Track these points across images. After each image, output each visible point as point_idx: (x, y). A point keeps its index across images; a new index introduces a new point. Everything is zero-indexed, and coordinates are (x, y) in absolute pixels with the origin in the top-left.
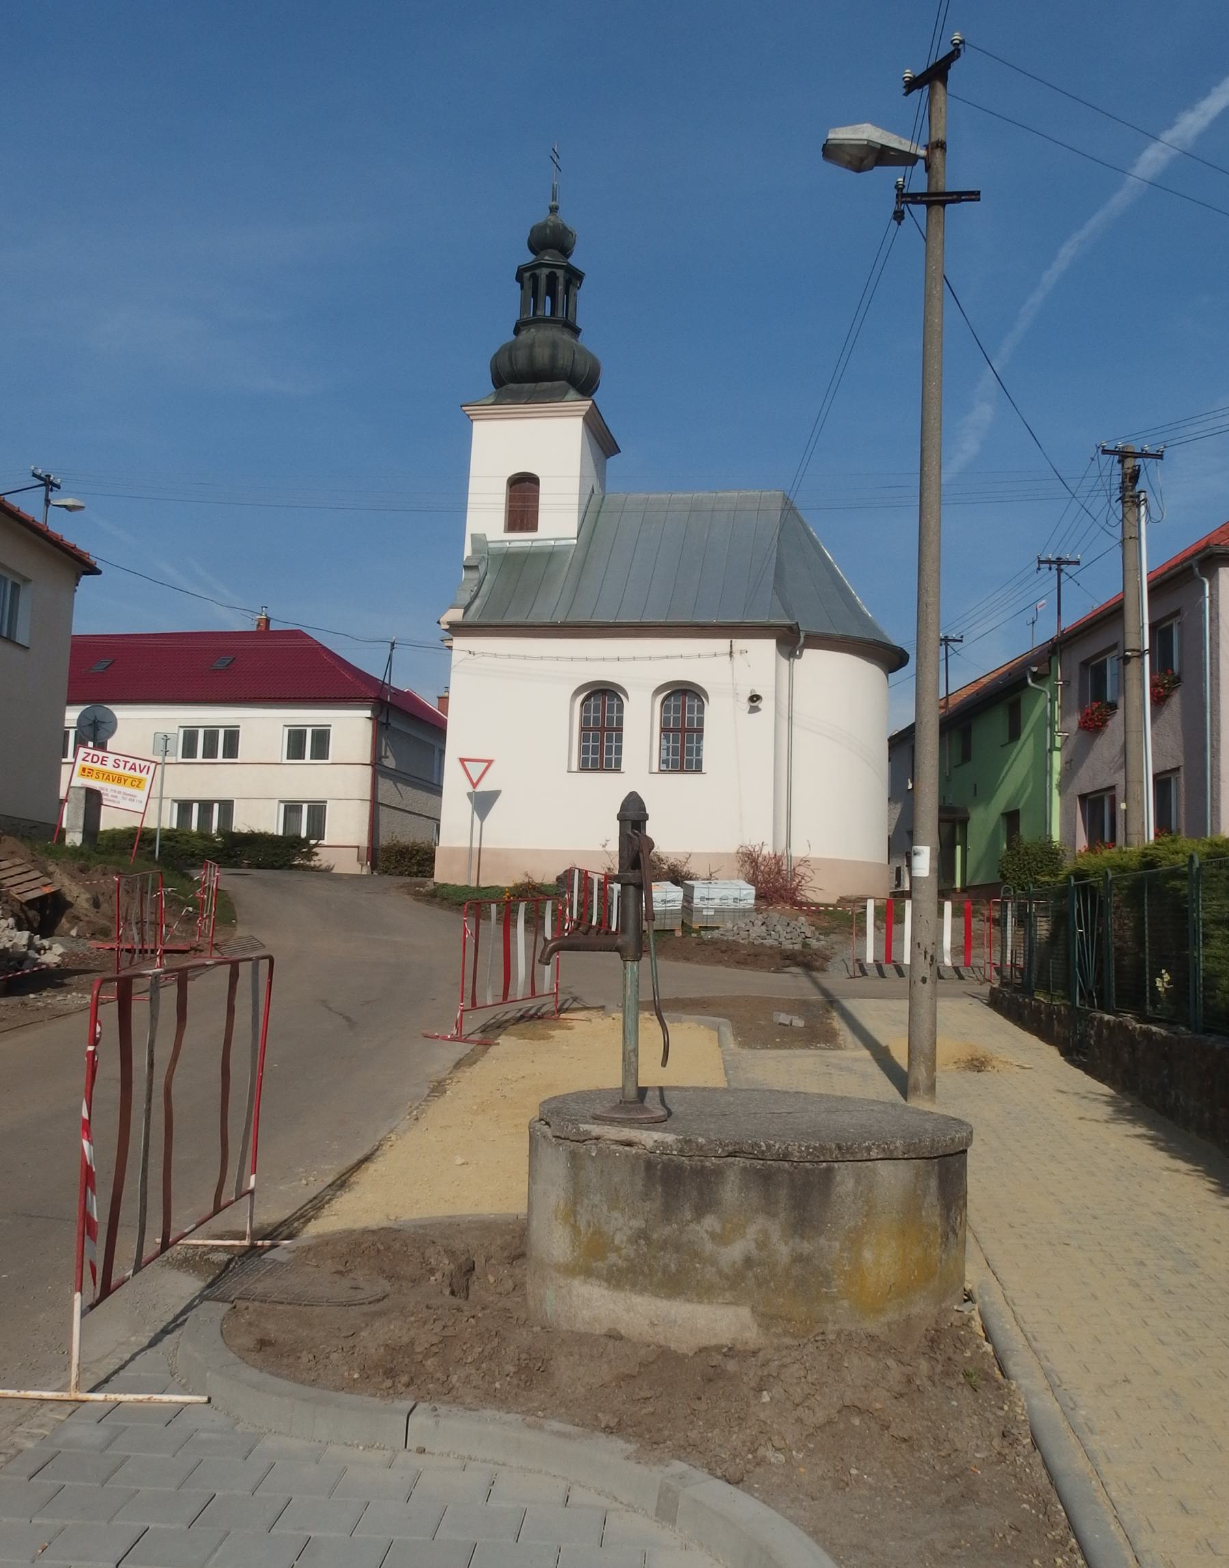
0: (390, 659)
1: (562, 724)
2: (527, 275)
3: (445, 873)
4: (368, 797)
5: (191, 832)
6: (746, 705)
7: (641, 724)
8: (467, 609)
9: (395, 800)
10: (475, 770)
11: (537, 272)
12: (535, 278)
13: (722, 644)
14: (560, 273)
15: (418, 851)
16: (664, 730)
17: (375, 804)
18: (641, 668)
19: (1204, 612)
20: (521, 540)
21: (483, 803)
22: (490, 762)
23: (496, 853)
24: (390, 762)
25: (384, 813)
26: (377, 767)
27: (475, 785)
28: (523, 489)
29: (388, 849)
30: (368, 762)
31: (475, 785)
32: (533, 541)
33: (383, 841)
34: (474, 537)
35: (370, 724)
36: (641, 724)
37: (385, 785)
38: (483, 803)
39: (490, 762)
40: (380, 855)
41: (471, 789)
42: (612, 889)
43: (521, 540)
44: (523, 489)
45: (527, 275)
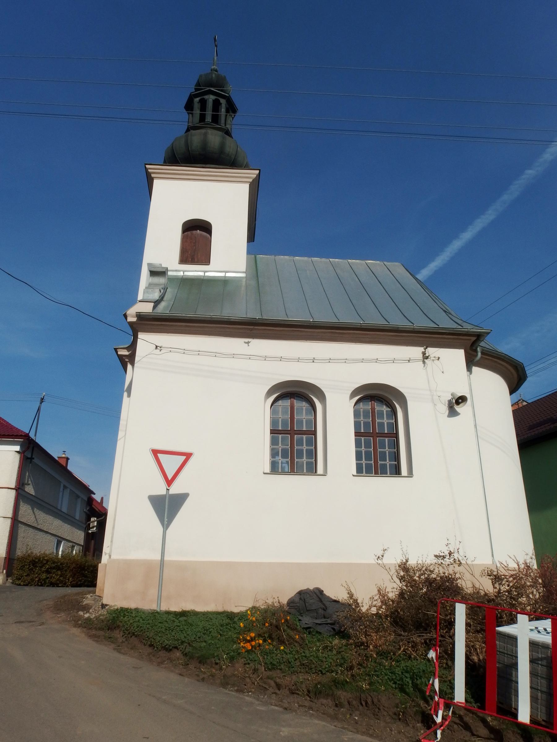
0: (39, 410)
1: (257, 419)
2: (197, 99)
3: (115, 589)
4: (10, 514)
5: (58, 559)
6: (445, 409)
7: (338, 427)
8: (157, 303)
9: (30, 520)
10: (171, 464)
11: (206, 97)
12: (203, 103)
13: (416, 351)
14: (223, 101)
15: (47, 561)
16: (358, 434)
17: (15, 522)
18: (340, 370)
19: (168, 506)
20: (194, 271)
21: (167, 507)
22: (188, 456)
23: (182, 567)
24: (30, 489)
25: (22, 529)
26: (20, 491)
27: (169, 482)
28: (196, 236)
29: (22, 559)
30: (13, 487)
31: (169, 482)
32: (205, 272)
33: (20, 552)
34: (149, 265)
35: (17, 457)
36: (338, 427)
37: (25, 508)
38: (167, 507)
39: (188, 456)
40: (16, 564)
41: (160, 489)
42: (513, 640)
43: (194, 271)
44: (196, 236)
45: (197, 99)
